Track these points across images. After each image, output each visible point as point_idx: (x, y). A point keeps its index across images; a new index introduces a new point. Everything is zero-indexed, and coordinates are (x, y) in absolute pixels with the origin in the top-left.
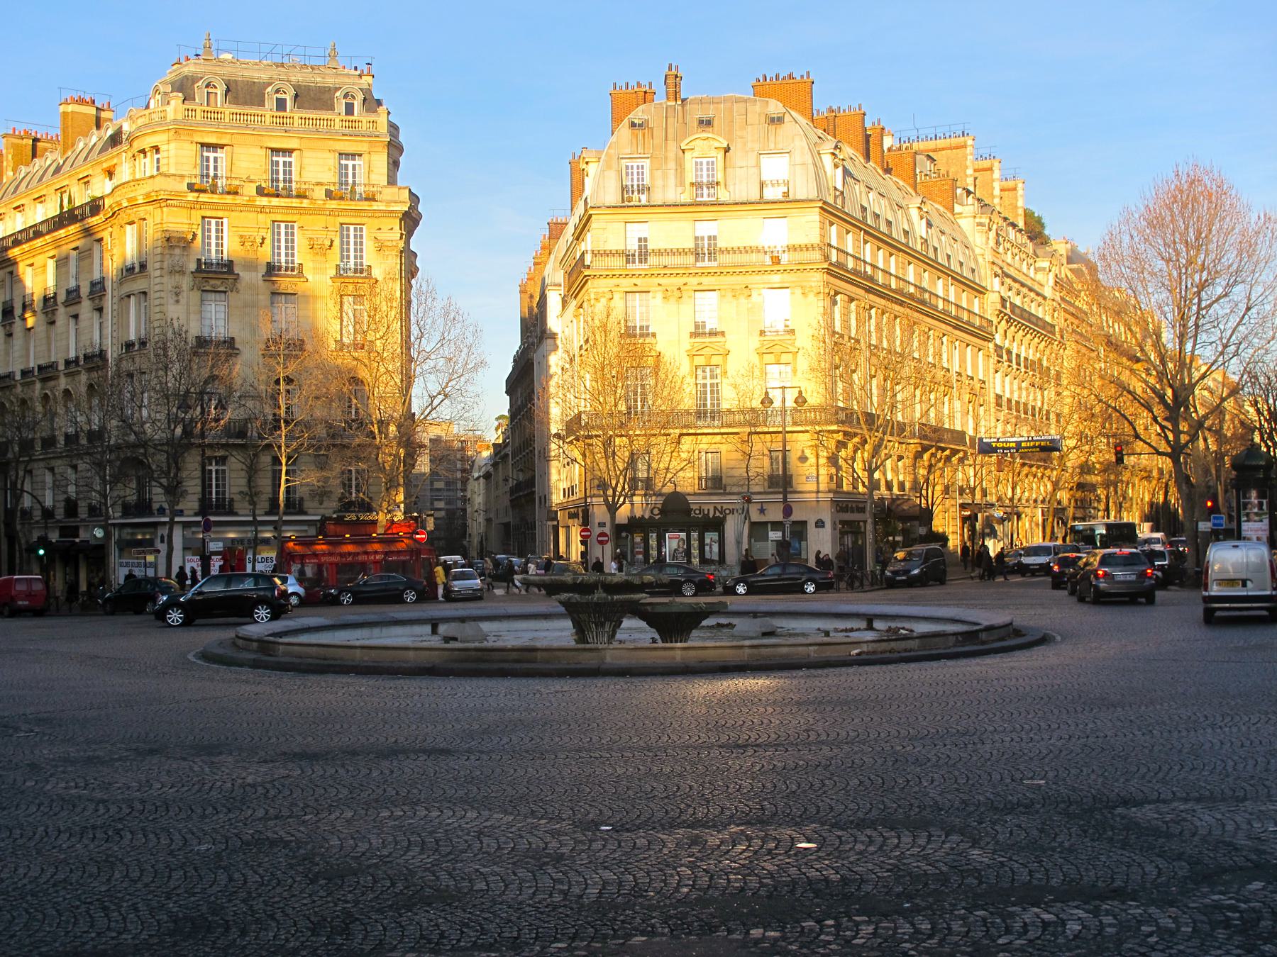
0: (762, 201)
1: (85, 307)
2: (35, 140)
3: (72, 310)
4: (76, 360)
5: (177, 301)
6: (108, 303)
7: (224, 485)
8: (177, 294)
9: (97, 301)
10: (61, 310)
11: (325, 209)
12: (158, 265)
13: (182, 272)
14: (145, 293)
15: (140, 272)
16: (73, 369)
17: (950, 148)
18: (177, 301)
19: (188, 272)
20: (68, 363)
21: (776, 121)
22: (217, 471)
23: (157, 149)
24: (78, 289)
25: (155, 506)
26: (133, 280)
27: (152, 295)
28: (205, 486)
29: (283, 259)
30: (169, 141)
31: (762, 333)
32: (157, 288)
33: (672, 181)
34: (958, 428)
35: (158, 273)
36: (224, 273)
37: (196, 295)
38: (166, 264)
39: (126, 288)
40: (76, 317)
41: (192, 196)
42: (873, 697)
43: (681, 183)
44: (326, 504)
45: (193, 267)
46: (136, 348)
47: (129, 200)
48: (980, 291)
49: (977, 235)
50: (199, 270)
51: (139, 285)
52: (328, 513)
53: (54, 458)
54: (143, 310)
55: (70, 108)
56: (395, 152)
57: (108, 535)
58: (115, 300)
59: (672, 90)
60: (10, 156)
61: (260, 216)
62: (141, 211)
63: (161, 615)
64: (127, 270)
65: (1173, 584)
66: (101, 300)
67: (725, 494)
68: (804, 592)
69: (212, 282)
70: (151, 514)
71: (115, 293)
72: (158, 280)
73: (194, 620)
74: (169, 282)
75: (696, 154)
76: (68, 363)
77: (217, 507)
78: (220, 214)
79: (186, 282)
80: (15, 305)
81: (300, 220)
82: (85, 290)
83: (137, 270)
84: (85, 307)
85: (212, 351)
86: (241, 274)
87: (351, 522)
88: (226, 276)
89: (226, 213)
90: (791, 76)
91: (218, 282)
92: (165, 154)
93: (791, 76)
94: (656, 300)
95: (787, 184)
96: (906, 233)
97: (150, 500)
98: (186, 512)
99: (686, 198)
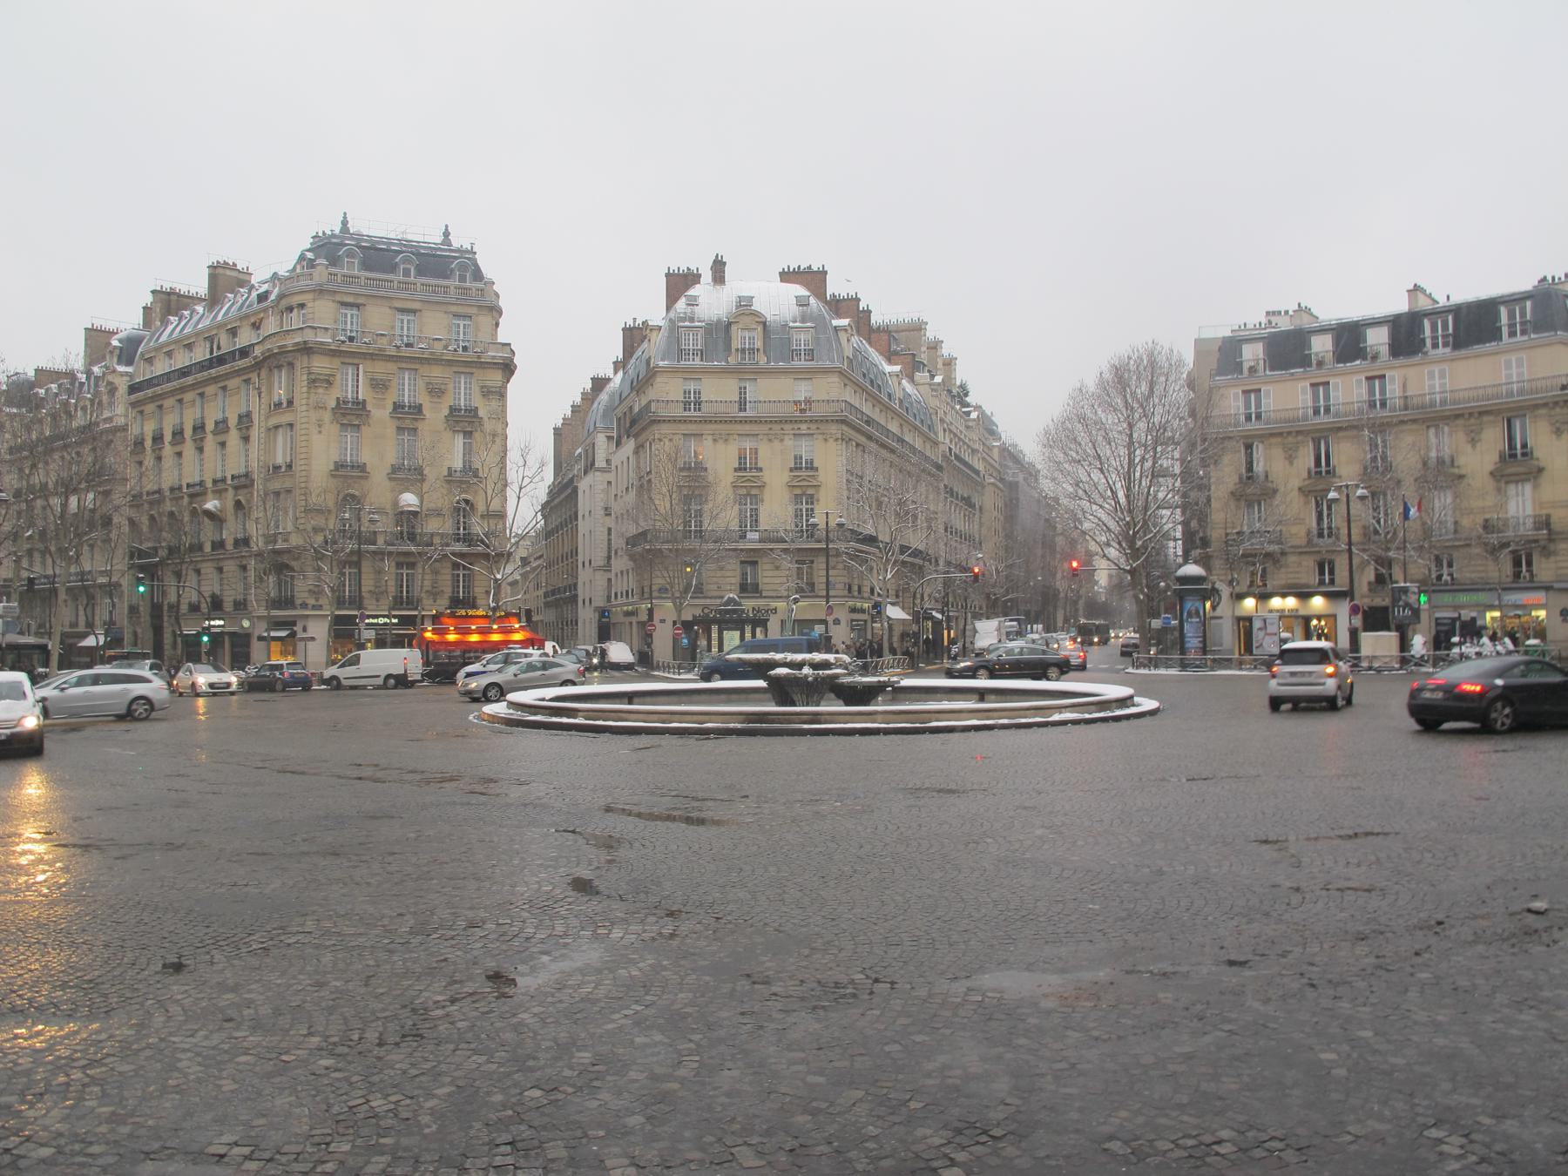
1: (233, 438)
3: (221, 438)
4: (224, 480)
5: (320, 432)
6: (254, 433)
7: (413, 585)
8: (320, 426)
9: (244, 431)
10: (210, 437)
12: (304, 402)
15: (288, 406)
16: (221, 486)
18: (320, 432)
19: (329, 408)
20: (215, 482)
23: (302, 306)
24: (225, 421)
25: (298, 602)
26: (282, 413)
27: (297, 427)
29: (406, 401)
30: (314, 300)
32: (303, 420)
34: (26, 582)
36: (359, 409)
37: (335, 428)
38: (311, 401)
39: (273, 421)
44: (438, 602)
45: (333, 404)
46: (283, 470)
47: (280, 347)
51: (285, 418)
52: (441, 609)
53: (202, 561)
54: (289, 439)
57: (253, 625)
58: (262, 430)
64: (275, 405)
65: (96, 664)
66: (248, 428)
67: (761, 597)
69: (348, 417)
70: (295, 608)
71: (262, 424)
73: (1441, 723)
74: (314, 415)
76: (215, 482)
78: (356, 361)
79: (327, 416)
80: (146, 438)
82: (233, 422)
83: (285, 405)
84: (233, 438)
85: (1515, 386)
86: (373, 411)
87: (462, 617)
88: (360, 412)
89: (361, 361)
91: (353, 417)
92: (310, 310)
94: (708, 442)
96: (889, 395)
97: (293, 596)
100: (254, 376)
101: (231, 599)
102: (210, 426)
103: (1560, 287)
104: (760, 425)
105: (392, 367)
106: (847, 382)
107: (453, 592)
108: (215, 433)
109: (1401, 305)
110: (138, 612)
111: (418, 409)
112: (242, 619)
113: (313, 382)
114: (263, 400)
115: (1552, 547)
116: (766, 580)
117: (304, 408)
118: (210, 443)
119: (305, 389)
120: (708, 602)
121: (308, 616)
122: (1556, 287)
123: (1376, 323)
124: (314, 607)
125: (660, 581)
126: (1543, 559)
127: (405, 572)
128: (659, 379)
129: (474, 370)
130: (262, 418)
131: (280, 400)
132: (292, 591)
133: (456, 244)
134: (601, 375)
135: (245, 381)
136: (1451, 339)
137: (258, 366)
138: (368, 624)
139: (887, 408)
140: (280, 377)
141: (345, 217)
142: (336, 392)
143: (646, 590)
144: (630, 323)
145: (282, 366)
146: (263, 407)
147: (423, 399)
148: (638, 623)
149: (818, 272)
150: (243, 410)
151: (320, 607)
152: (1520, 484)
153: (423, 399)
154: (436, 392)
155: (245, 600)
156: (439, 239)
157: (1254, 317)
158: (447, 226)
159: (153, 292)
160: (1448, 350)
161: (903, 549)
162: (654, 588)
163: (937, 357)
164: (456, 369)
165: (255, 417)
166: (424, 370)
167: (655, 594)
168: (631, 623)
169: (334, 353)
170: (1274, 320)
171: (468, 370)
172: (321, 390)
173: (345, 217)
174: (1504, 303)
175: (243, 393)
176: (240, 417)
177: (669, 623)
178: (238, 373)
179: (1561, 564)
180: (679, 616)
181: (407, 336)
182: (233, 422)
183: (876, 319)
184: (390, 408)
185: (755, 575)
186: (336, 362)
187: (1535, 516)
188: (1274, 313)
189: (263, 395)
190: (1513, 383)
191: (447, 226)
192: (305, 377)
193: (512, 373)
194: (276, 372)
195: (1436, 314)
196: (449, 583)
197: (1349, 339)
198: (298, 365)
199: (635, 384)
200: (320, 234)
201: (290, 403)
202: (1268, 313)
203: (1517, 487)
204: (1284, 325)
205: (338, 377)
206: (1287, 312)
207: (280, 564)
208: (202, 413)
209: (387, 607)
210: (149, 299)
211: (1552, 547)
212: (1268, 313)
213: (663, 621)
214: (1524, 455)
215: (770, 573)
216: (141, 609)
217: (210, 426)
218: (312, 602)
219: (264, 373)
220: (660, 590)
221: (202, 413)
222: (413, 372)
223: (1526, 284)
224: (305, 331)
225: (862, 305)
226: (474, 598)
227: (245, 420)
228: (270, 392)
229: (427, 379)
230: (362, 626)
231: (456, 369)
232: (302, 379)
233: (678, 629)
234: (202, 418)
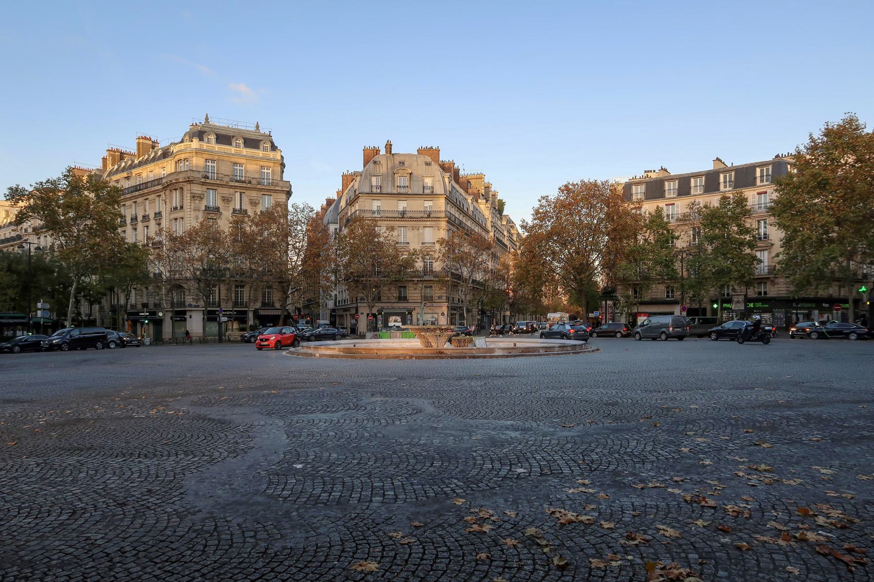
0: (372, 193)
2: (121, 153)
3: (146, 224)
8: (197, 219)
11: (256, 188)
12: (189, 207)
13: (199, 210)
14: (182, 218)
17: (476, 179)
21: (428, 164)
22: (241, 291)
25: (187, 304)
28: (237, 297)
31: (423, 243)
32: (188, 216)
33: (390, 184)
35: (189, 210)
39: (174, 216)
40: (147, 227)
41: (203, 180)
42: (548, 374)
43: (393, 185)
45: (203, 208)
47: (176, 180)
48: (488, 232)
49: (487, 211)
50: (206, 210)
55: (141, 141)
56: (283, 167)
57: (164, 315)
59: (389, 150)
60: (110, 160)
61: (231, 189)
62: (181, 185)
63: (634, 337)
66: (160, 219)
67: (408, 303)
68: (110, 348)
69: (211, 215)
70: (186, 307)
71: (168, 218)
72: (188, 213)
75: (399, 175)
77: (213, 304)
78: (214, 188)
81: (248, 192)
82: (152, 216)
83: (179, 208)
90: (432, 148)
91: (214, 215)
93: (432, 148)
95: (433, 187)
97: (184, 301)
98: (200, 306)
99: (395, 192)
100: (162, 194)
101: (153, 302)
102: (140, 218)
103: (785, 159)
104: (408, 222)
105: (232, 191)
106: (448, 202)
107: (263, 299)
108: (142, 222)
109: (710, 167)
110: (104, 309)
111: (218, 209)
112: (159, 312)
113: (193, 197)
114: (167, 206)
115: (776, 281)
116: (410, 295)
117: (189, 210)
118: (140, 226)
119: (189, 201)
120: (293, 523)
121: (192, 310)
122: (785, 159)
123: (697, 175)
124: (195, 306)
125: (361, 295)
126: (772, 287)
127: (239, 289)
128: (360, 200)
129: (272, 194)
130: (167, 215)
131: (176, 206)
132: (184, 298)
133: (262, 131)
134: (331, 197)
135: (158, 196)
136: (770, 178)
137: (165, 188)
138: (223, 314)
139: (466, 214)
140: (176, 194)
141: (207, 116)
142: (204, 203)
143: (354, 299)
144: (346, 172)
145: (177, 189)
146: (167, 209)
147: (219, 203)
148: (350, 314)
149: (436, 150)
150: (157, 211)
151: (198, 306)
152: (762, 252)
153: (219, 203)
154: (226, 200)
155: (160, 303)
156: (253, 129)
157: (640, 174)
158: (258, 123)
159: (108, 150)
160: (731, 189)
161: (474, 281)
162: (358, 298)
163: (489, 191)
164: (263, 193)
165: (163, 214)
166: (221, 190)
167: (359, 301)
168: (347, 315)
169: (204, 184)
170: (649, 174)
171: (269, 193)
172: (197, 202)
173: (207, 116)
174: (758, 166)
175: (157, 202)
176: (156, 214)
177: (365, 314)
178: (154, 192)
179: (780, 289)
180: (371, 311)
181: (245, 177)
182: (152, 216)
183: (461, 173)
184: (231, 211)
185: (405, 292)
186: (205, 188)
187: (769, 266)
188: (648, 171)
189: (167, 203)
190: (761, 204)
191: (258, 123)
192: (189, 195)
193: (290, 195)
194: (174, 192)
195: (727, 170)
196: (261, 295)
197: (684, 185)
198: (185, 188)
199: (348, 202)
200: (194, 125)
201: (182, 207)
202: (645, 172)
203: (176, 192)
204: (653, 176)
205: (261, 201)
206: (654, 171)
207: (177, 286)
208: (136, 211)
209: (231, 306)
210: (105, 154)
211: (776, 281)
212: (645, 172)
213: (362, 314)
214: (764, 238)
215: (413, 292)
216: (105, 307)
217: (140, 218)
218: (194, 304)
219: (168, 192)
220: (361, 299)
221: (136, 211)
222: (214, 191)
223: (770, 158)
224: (189, 172)
225: (456, 166)
226: (273, 303)
227: (158, 215)
228: (171, 202)
229: (249, 198)
230: (221, 315)
231: (263, 193)
232: (187, 196)
233: (370, 317)
234: (136, 214)
